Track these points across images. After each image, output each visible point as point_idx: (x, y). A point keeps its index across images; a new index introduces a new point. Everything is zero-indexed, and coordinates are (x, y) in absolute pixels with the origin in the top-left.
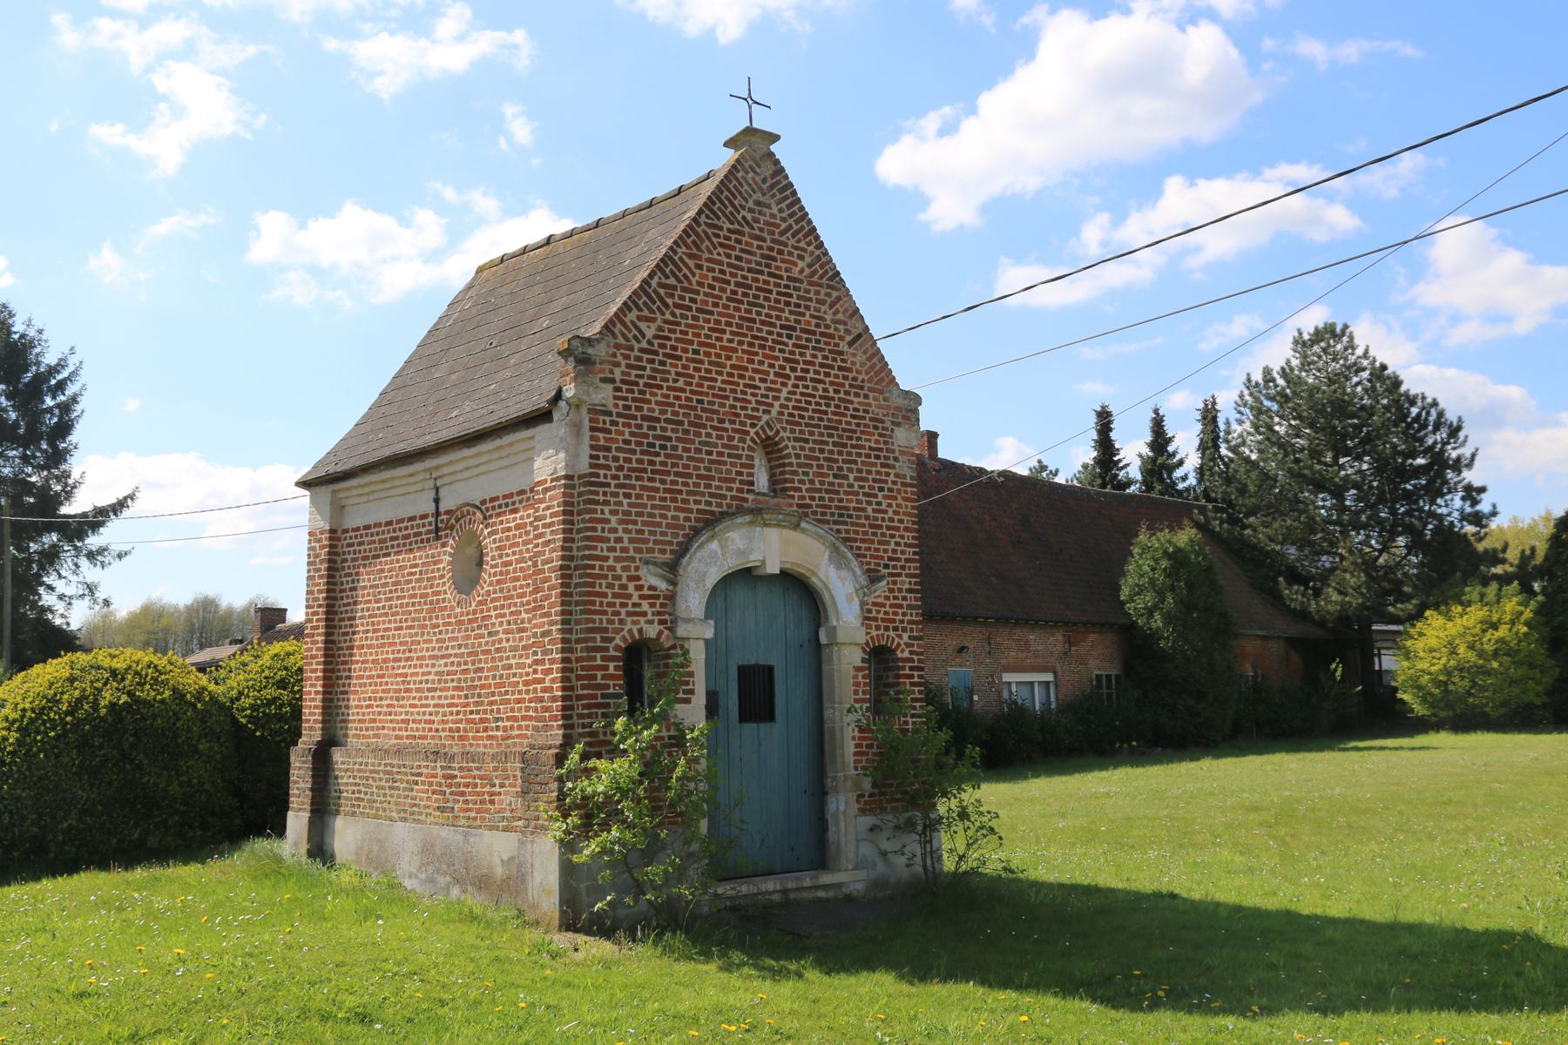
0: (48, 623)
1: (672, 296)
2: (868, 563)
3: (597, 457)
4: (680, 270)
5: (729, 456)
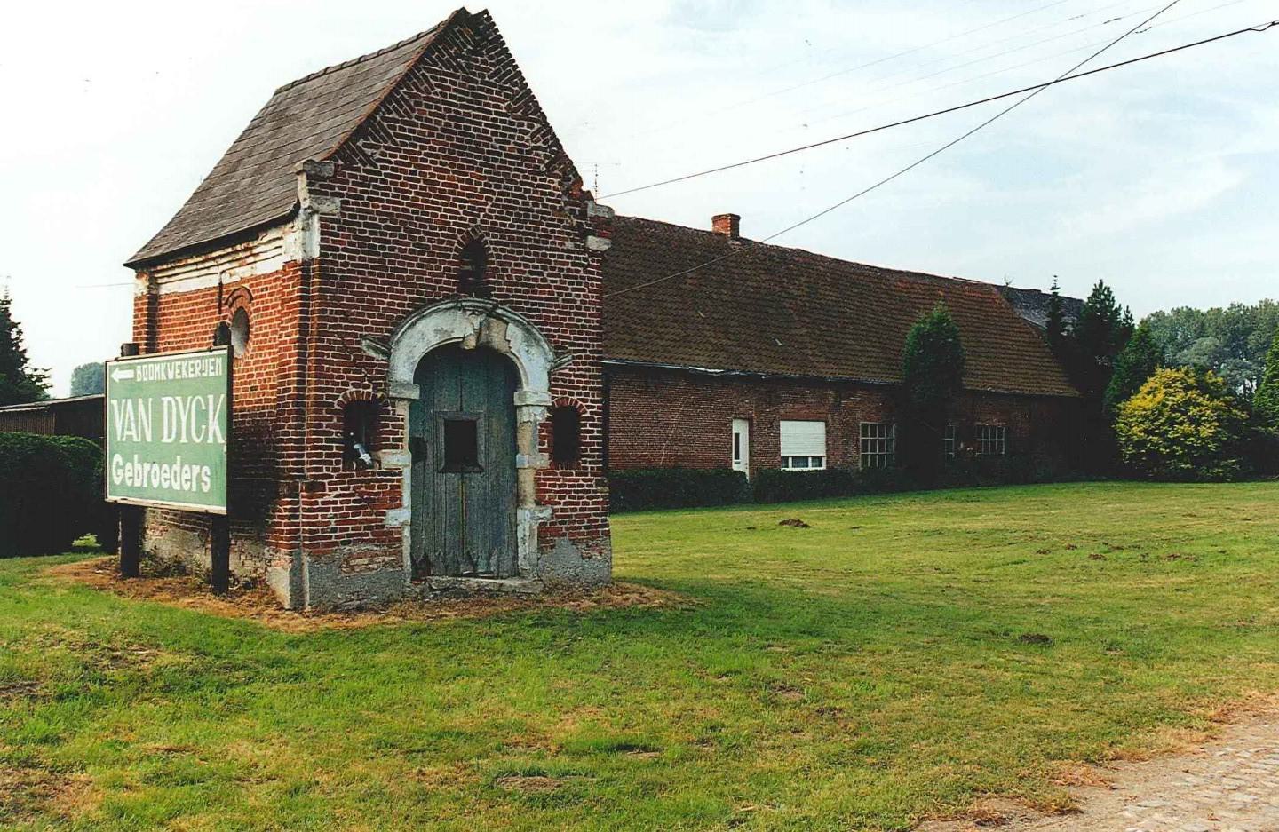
0: (276, 497)
1: (394, 128)
2: (556, 342)
3: (327, 255)
4: (401, 107)
5: (439, 255)
